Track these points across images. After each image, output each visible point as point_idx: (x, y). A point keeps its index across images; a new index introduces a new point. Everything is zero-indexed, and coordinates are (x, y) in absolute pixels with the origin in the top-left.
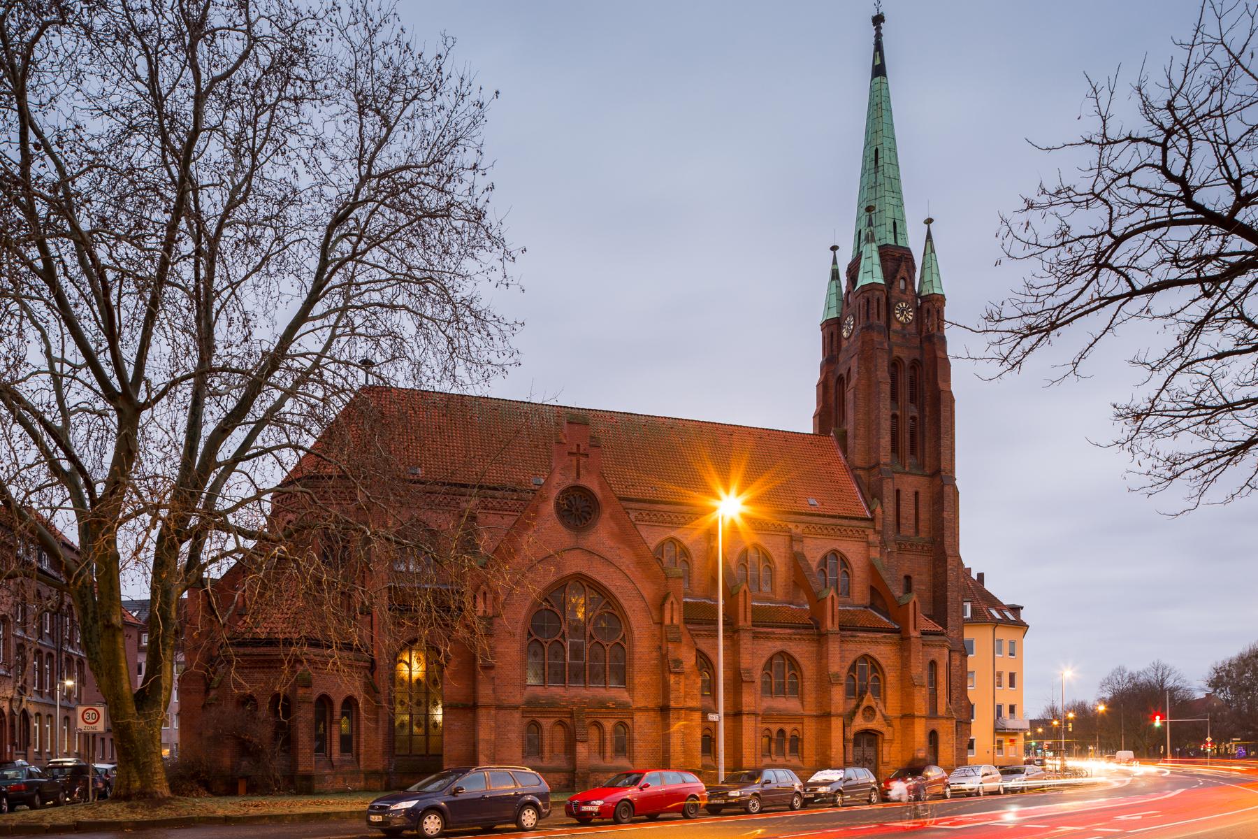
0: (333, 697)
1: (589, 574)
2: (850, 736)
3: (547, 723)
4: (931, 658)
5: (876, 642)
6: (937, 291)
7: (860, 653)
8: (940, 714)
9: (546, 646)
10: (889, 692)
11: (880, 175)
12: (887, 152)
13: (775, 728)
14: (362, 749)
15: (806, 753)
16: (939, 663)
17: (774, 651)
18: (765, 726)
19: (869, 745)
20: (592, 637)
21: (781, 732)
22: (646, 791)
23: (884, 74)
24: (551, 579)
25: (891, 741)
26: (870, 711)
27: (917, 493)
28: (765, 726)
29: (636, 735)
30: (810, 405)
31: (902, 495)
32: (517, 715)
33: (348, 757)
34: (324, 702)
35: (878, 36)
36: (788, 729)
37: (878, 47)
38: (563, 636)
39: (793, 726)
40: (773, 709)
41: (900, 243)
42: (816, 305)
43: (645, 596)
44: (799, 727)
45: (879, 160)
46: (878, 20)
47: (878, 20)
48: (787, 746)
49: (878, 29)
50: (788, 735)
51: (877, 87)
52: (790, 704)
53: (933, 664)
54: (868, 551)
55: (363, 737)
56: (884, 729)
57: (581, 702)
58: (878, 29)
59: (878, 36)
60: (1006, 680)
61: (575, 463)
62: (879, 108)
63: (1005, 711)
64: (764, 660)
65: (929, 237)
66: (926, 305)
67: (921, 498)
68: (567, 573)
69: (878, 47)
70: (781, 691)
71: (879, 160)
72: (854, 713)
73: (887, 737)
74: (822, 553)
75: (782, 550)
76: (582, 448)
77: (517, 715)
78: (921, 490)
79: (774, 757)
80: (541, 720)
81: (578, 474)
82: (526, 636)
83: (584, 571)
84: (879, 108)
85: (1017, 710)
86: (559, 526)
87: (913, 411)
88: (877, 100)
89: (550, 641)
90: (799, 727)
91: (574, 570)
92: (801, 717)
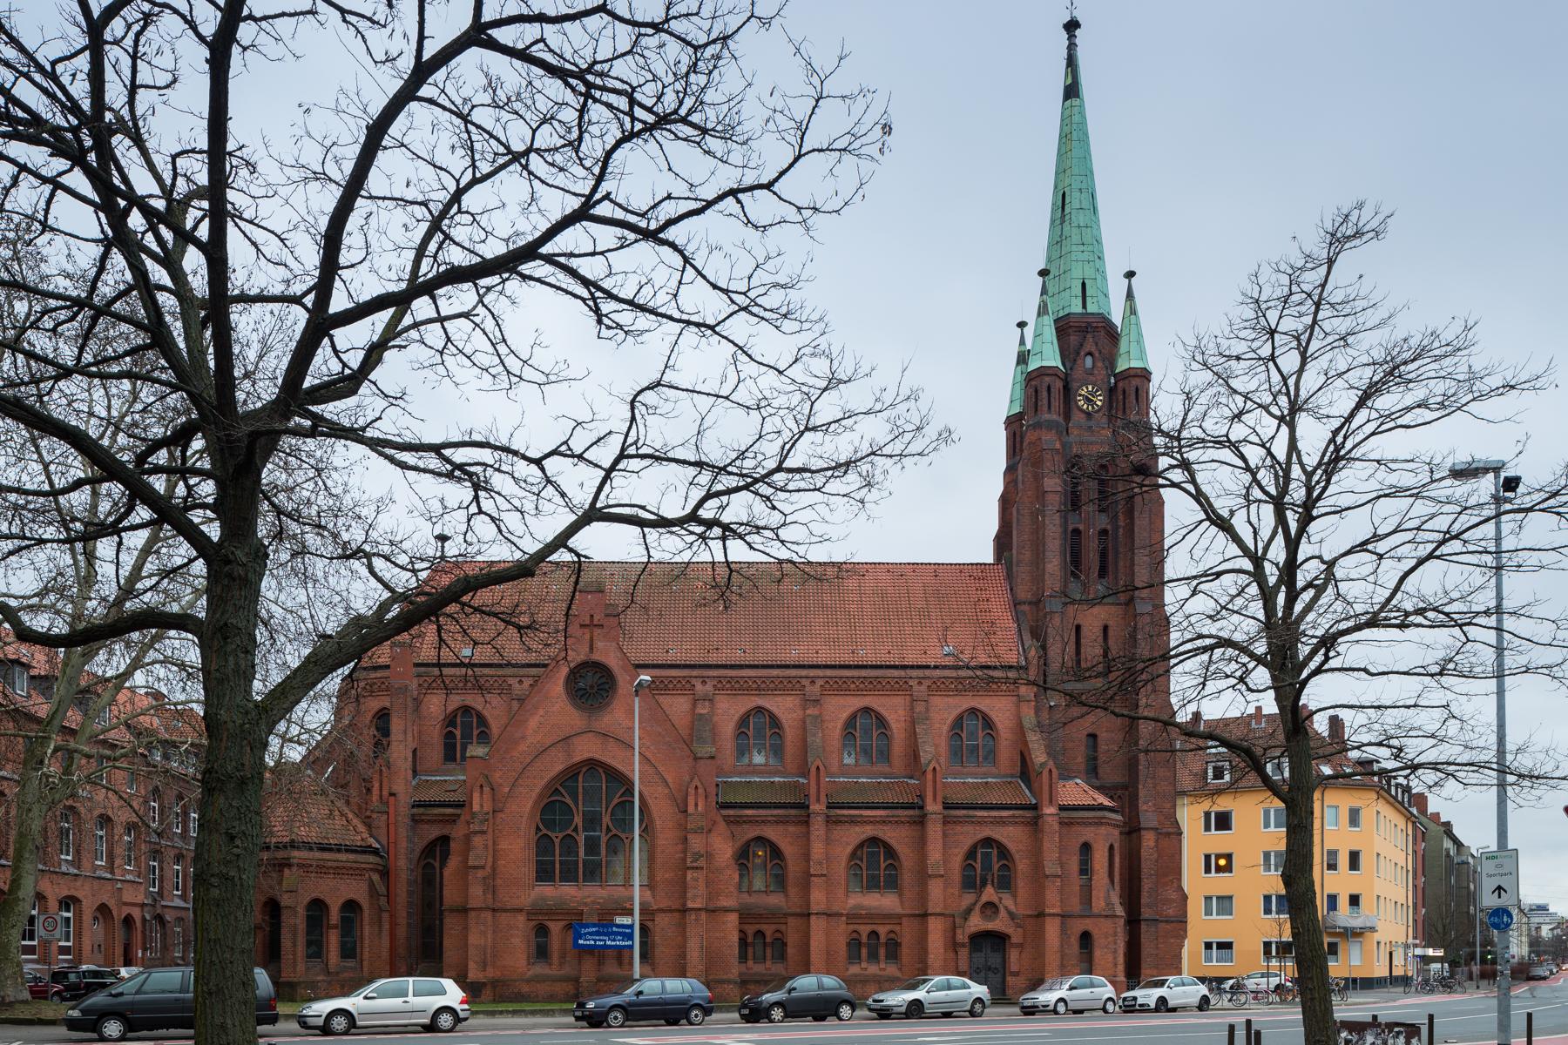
0: (328, 901)
1: (603, 759)
2: (962, 937)
3: (555, 927)
4: (1082, 840)
5: (1001, 822)
6: (1134, 364)
7: (980, 836)
8: (1095, 910)
9: (557, 841)
10: (1020, 883)
11: (1066, 227)
12: (1076, 194)
13: (864, 930)
14: (366, 955)
15: (905, 960)
16: (1095, 846)
17: (863, 837)
18: (852, 927)
19: (993, 950)
20: (608, 830)
21: (874, 934)
22: (120, 999)
23: (1077, 95)
24: (560, 767)
25: (1021, 946)
26: (991, 908)
27: (1106, 628)
28: (852, 927)
29: (657, 939)
30: (990, 524)
31: (1084, 632)
32: (521, 918)
33: (351, 963)
34: (317, 907)
35: (1072, 46)
36: (882, 930)
37: (1071, 62)
38: (576, 829)
39: (889, 927)
40: (862, 907)
41: (1091, 308)
42: (997, 395)
43: (670, 781)
44: (897, 928)
45: (1071, 207)
46: (1072, 26)
47: (1072, 26)
48: (882, 952)
49: (1071, 36)
50: (883, 939)
51: (1067, 112)
52: (885, 901)
53: (1086, 848)
54: (1018, 707)
55: (367, 942)
56: (1009, 930)
57: (594, 902)
58: (1071, 36)
59: (1072, 46)
60: (1343, 861)
61: (587, 637)
62: (1073, 142)
63: (1343, 902)
64: (849, 849)
65: (1130, 295)
66: (1121, 384)
67: (1111, 633)
68: (577, 759)
69: (1071, 62)
70: (873, 884)
71: (1071, 207)
72: (969, 911)
73: (1014, 940)
74: (955, 713)
75: (901, 712)
76: (596, 618)
77: (521, 918)
78: (1110, 623)
79: (864, 965)
80: (548, 924)
81: (591, 648)
82: (533, 831)
83: (597, 756)
84: (1073, 142)
85: (1362, 901)
86: (569, 708)
87: (1103, 521)
88: (1067, 129)
89: (561, 835)
90: (897, 928)
91: (586, 756)
92: (900, 916)
